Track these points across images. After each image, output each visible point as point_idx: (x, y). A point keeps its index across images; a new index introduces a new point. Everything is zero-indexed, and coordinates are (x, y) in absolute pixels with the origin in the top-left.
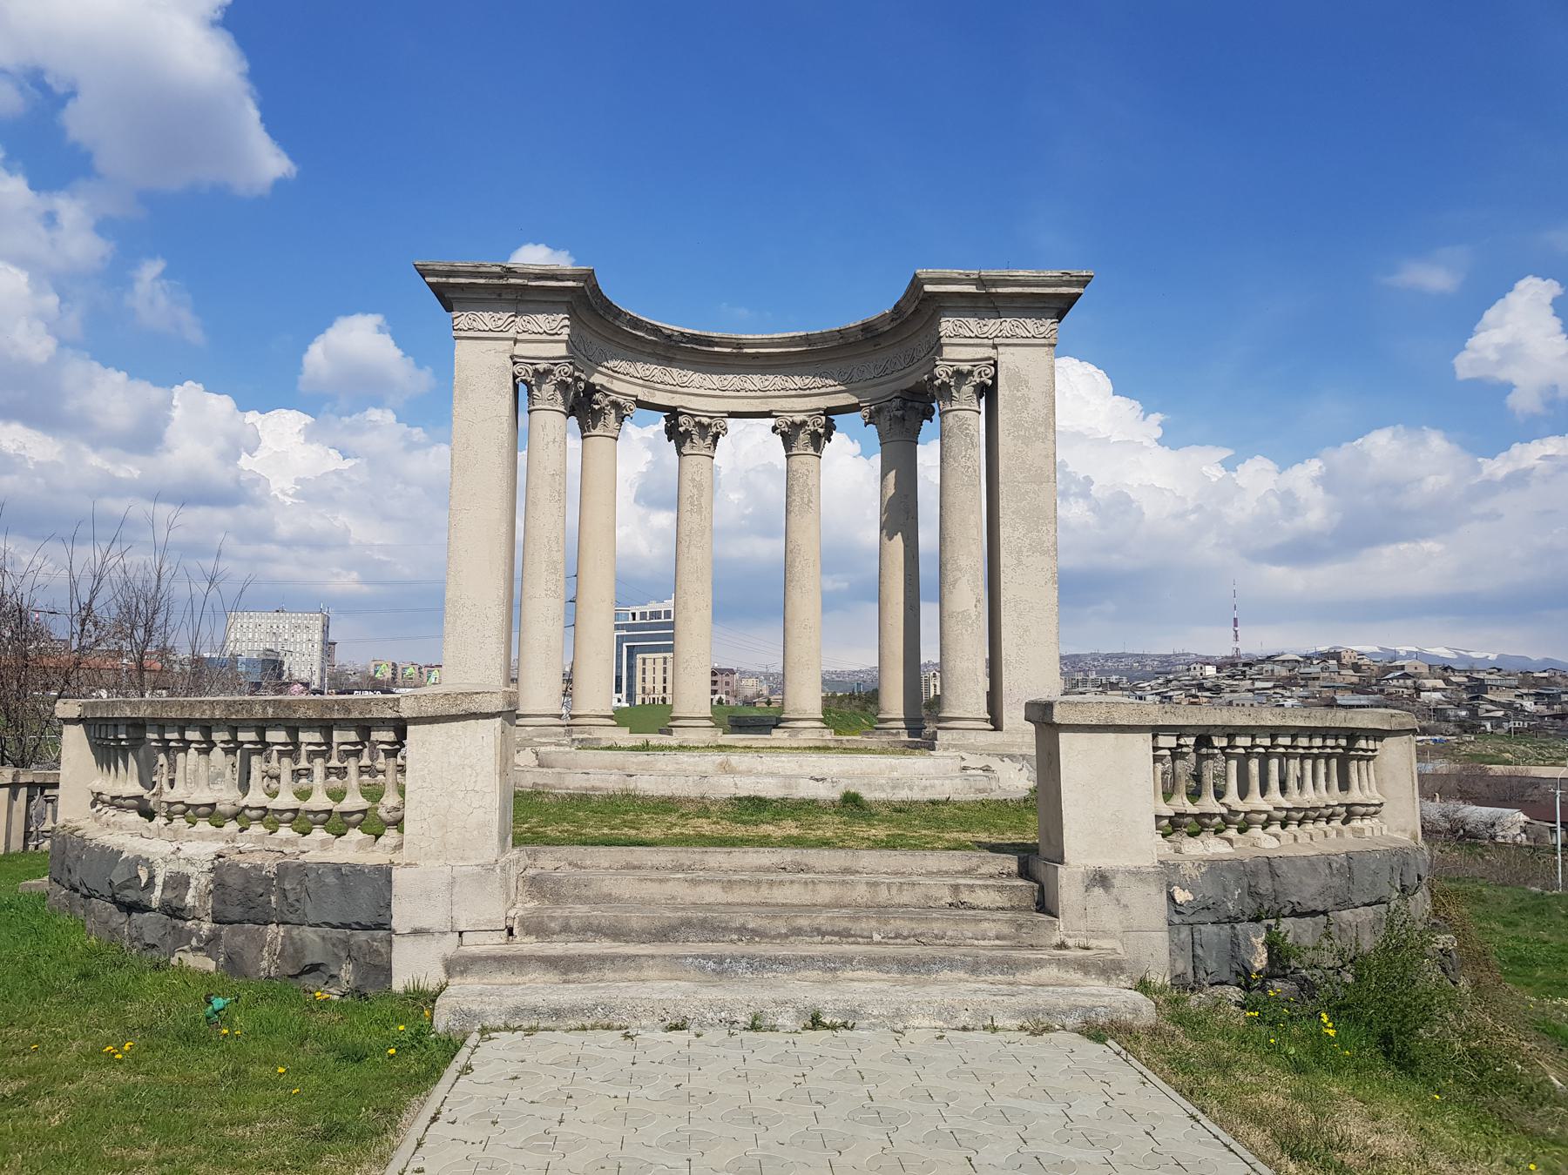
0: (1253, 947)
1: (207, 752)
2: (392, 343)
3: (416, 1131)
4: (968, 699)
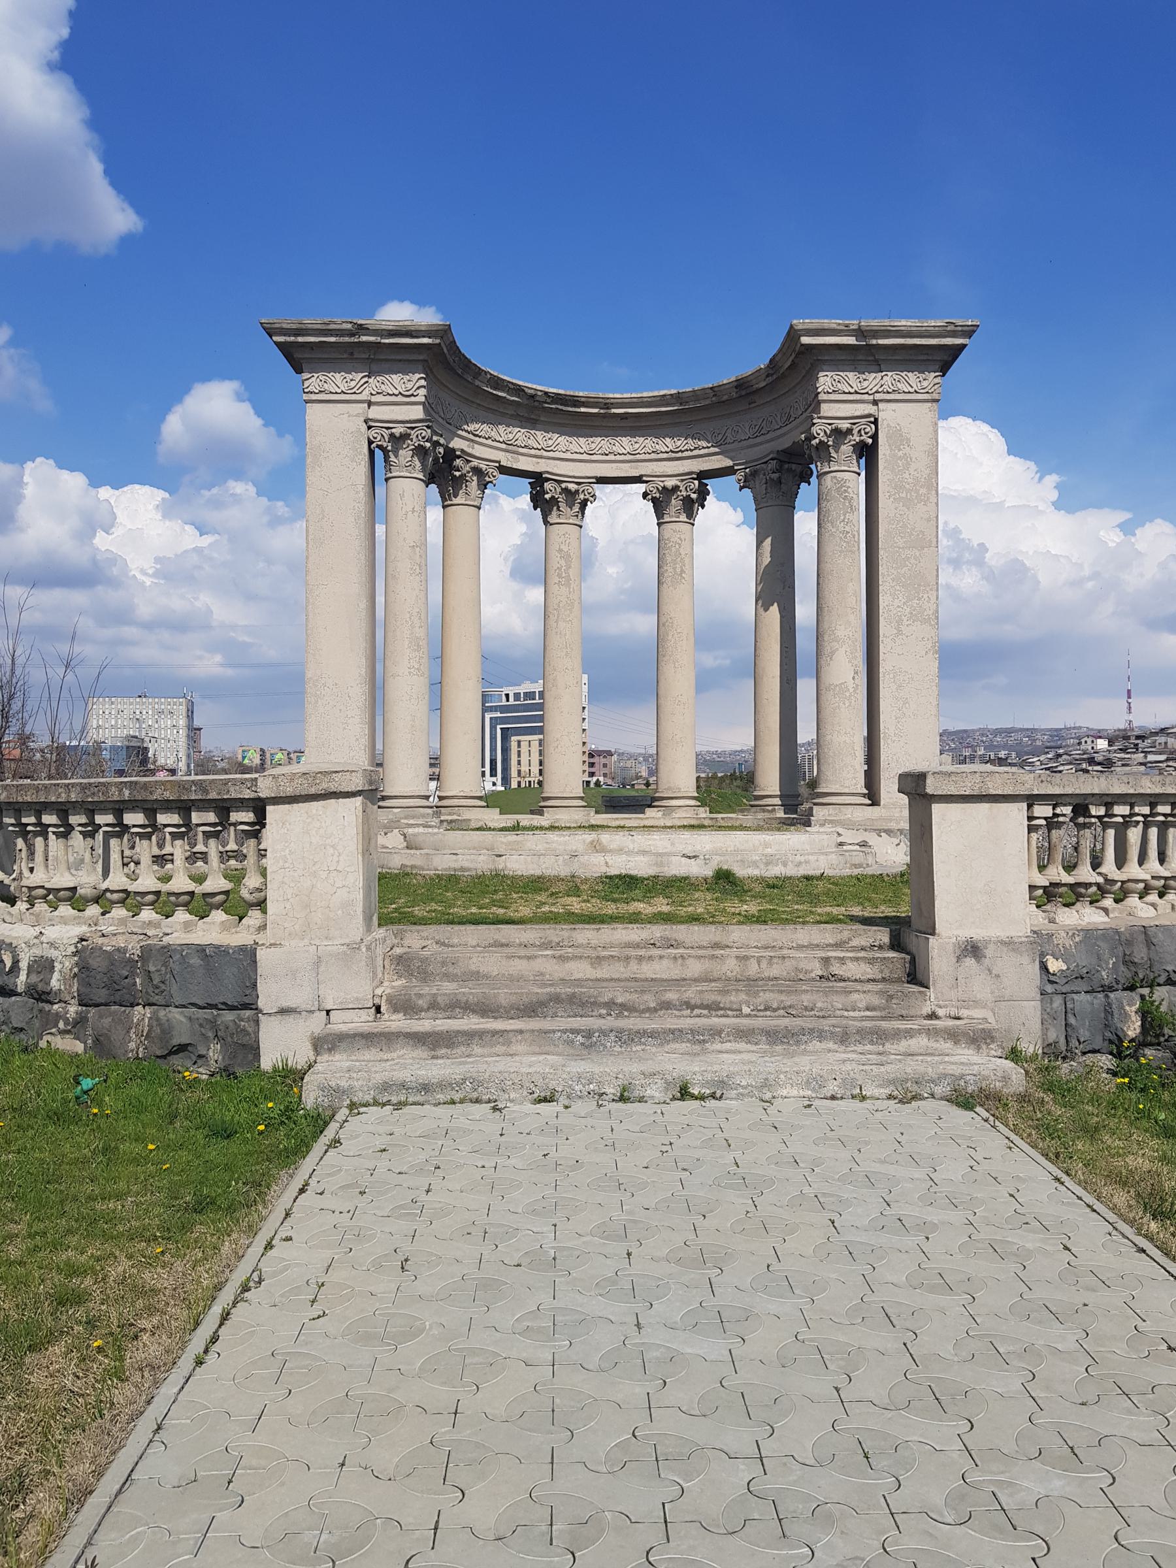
0: (1126, 1016)
1: (65, 835)
2: (252, 411)
3: (285, 1201)
4: (845, 773)
